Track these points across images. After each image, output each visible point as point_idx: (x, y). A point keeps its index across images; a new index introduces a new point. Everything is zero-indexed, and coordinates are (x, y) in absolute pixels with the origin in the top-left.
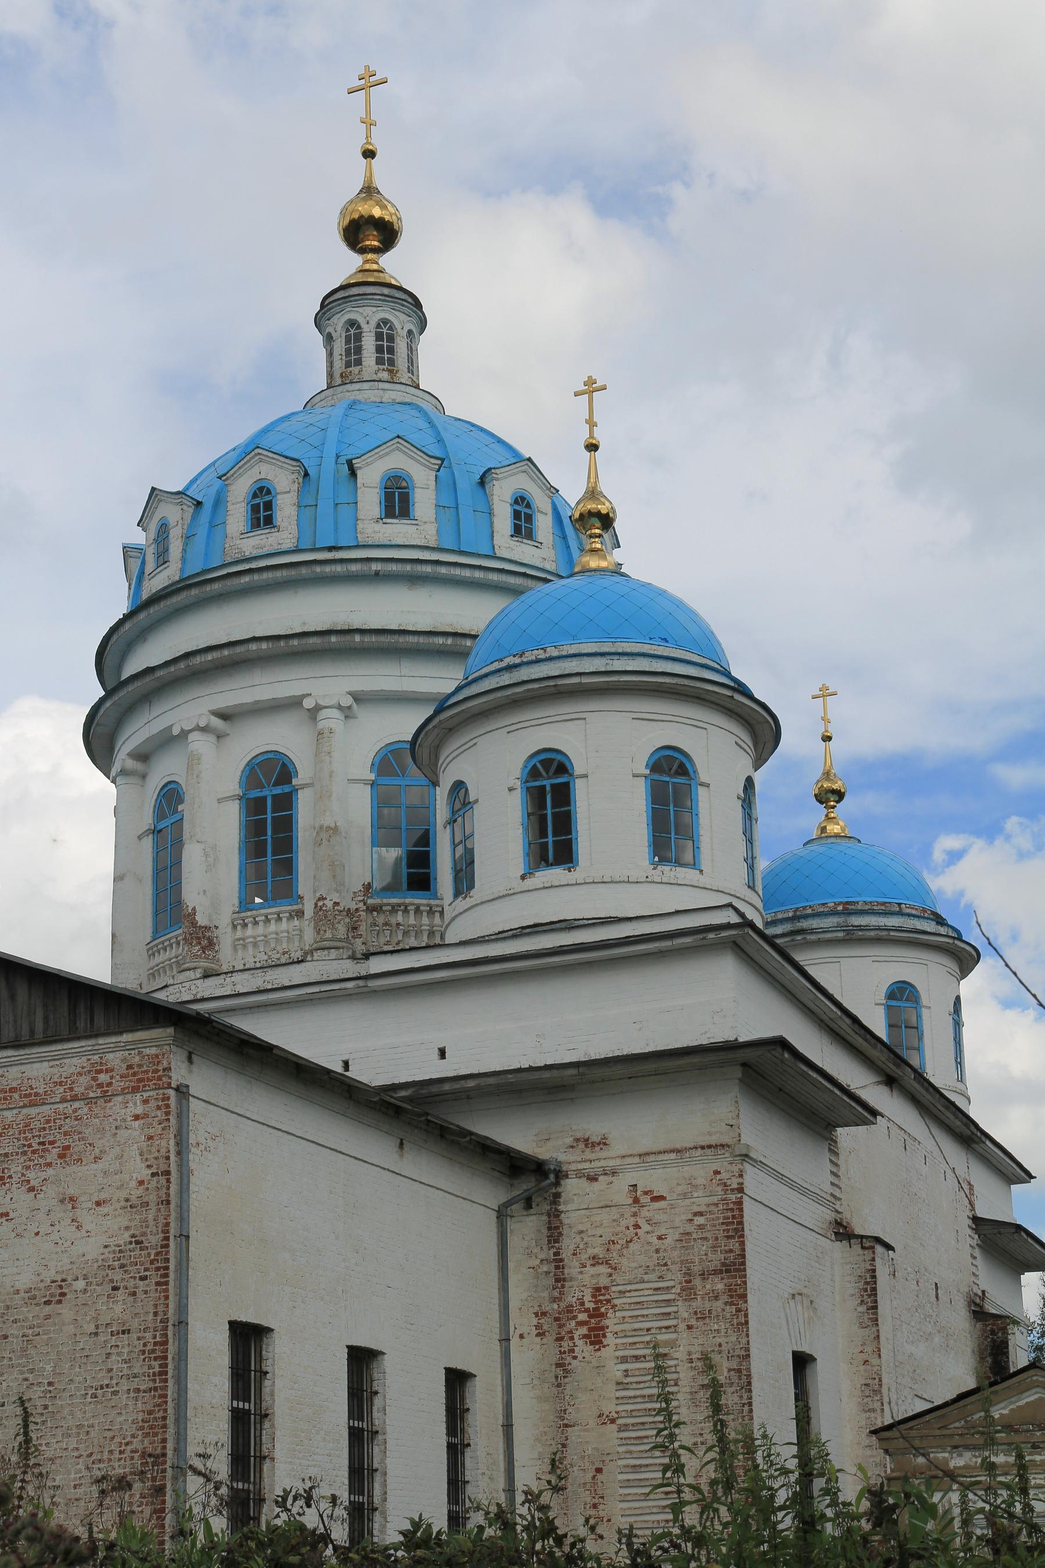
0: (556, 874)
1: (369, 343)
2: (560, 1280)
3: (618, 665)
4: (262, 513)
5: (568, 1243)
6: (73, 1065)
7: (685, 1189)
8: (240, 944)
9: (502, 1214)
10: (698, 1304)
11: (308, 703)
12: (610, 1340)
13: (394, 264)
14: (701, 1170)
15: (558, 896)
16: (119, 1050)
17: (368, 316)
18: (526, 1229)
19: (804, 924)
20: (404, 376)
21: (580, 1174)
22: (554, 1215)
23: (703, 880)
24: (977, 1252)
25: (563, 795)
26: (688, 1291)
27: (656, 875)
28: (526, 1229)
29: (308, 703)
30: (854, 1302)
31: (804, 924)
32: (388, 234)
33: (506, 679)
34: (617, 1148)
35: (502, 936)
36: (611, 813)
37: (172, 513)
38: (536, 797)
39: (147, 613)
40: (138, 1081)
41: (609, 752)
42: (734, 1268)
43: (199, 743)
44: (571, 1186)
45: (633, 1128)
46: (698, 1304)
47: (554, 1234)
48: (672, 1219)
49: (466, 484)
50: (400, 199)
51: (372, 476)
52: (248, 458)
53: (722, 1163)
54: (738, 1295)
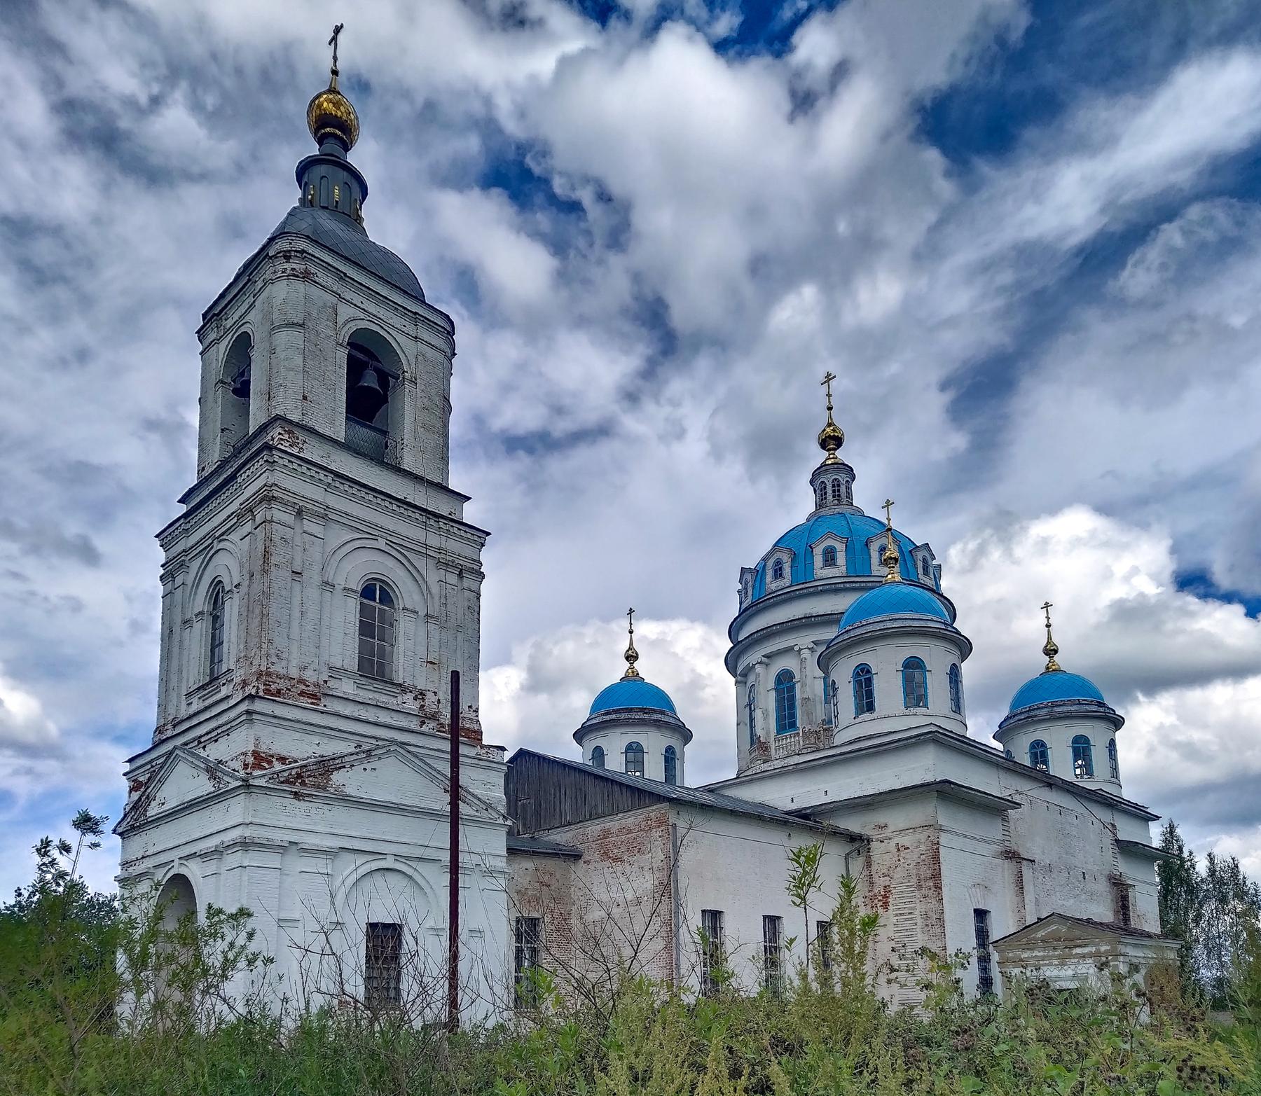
0: (867, 716)
1: (829, 490)
2: (872, 883)
3: (889, 625)
4: (778, 574)
5: (874, 868)
6: (631, 820)
7: (916, 843)
8: (777, 748)
9: (847, 857)
10: (923, 892)
11: (796, 648)
12: (891, 907)
13: (841, 454)
14: (922, 836)
15: (869, 726)
16: (655, 811)
17: (828, 479)
18: (857, 865)
19: (1033, 713)
20: (845, 501)
21: (877, 840)
22: (869, 857)
23: (929, 712)
24: (1118, 856)
25: (869, 681)
26: (920, 887)
27: (907, 712)
28: (857, 865)
29: (796, 648)
30: (1013, 886)
31: (1033, 713)
32: (838, 442)
33: (846, 636)
34: (891, 828)
35: (851, 743)
36: (888, 688)
37: (748, 576)
38: (858, 684)
39: (746, 615)
40: (661, 822)
41: (886, 663)
42: (936, 876)
43: (759, 669)
44: (874, 845)
45: (896, 819)
46: (923, 892)
47: (869, 865)
48: (912, 857)
49: (858, 546)
50: (843, 425)
51: (819, 550)
52: (225, 728)
53: (930, 832)
54: (938, 888)
